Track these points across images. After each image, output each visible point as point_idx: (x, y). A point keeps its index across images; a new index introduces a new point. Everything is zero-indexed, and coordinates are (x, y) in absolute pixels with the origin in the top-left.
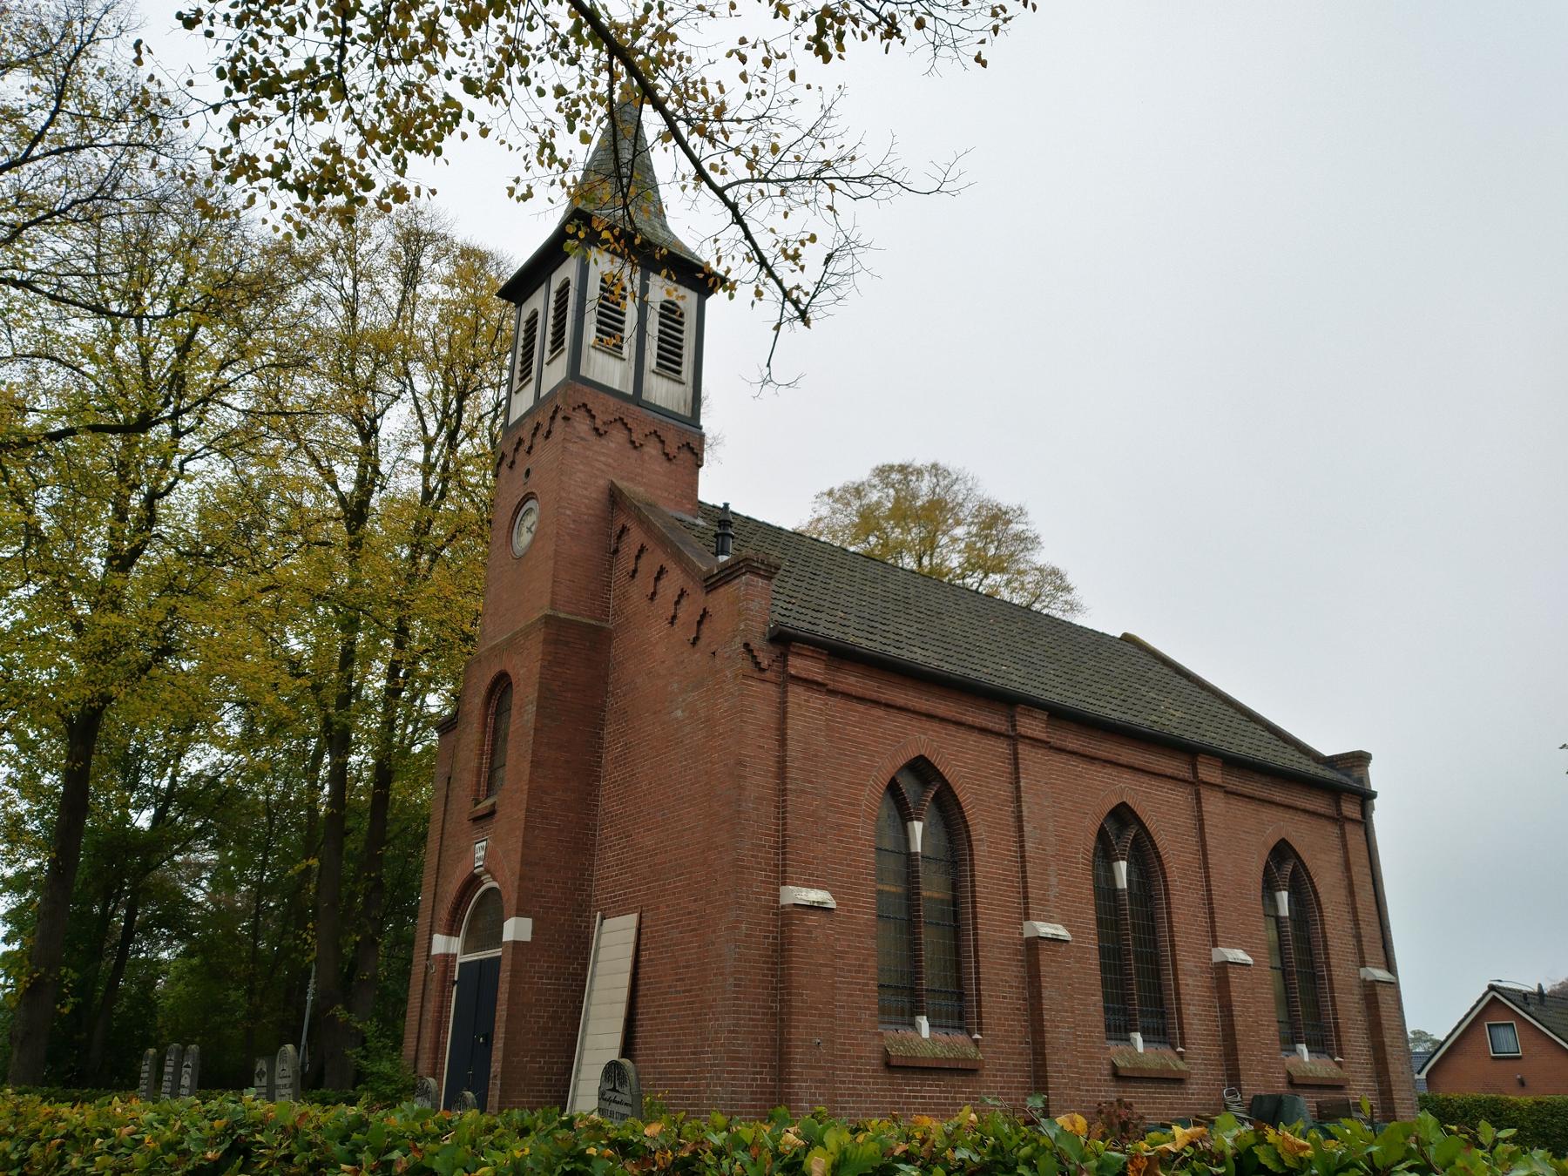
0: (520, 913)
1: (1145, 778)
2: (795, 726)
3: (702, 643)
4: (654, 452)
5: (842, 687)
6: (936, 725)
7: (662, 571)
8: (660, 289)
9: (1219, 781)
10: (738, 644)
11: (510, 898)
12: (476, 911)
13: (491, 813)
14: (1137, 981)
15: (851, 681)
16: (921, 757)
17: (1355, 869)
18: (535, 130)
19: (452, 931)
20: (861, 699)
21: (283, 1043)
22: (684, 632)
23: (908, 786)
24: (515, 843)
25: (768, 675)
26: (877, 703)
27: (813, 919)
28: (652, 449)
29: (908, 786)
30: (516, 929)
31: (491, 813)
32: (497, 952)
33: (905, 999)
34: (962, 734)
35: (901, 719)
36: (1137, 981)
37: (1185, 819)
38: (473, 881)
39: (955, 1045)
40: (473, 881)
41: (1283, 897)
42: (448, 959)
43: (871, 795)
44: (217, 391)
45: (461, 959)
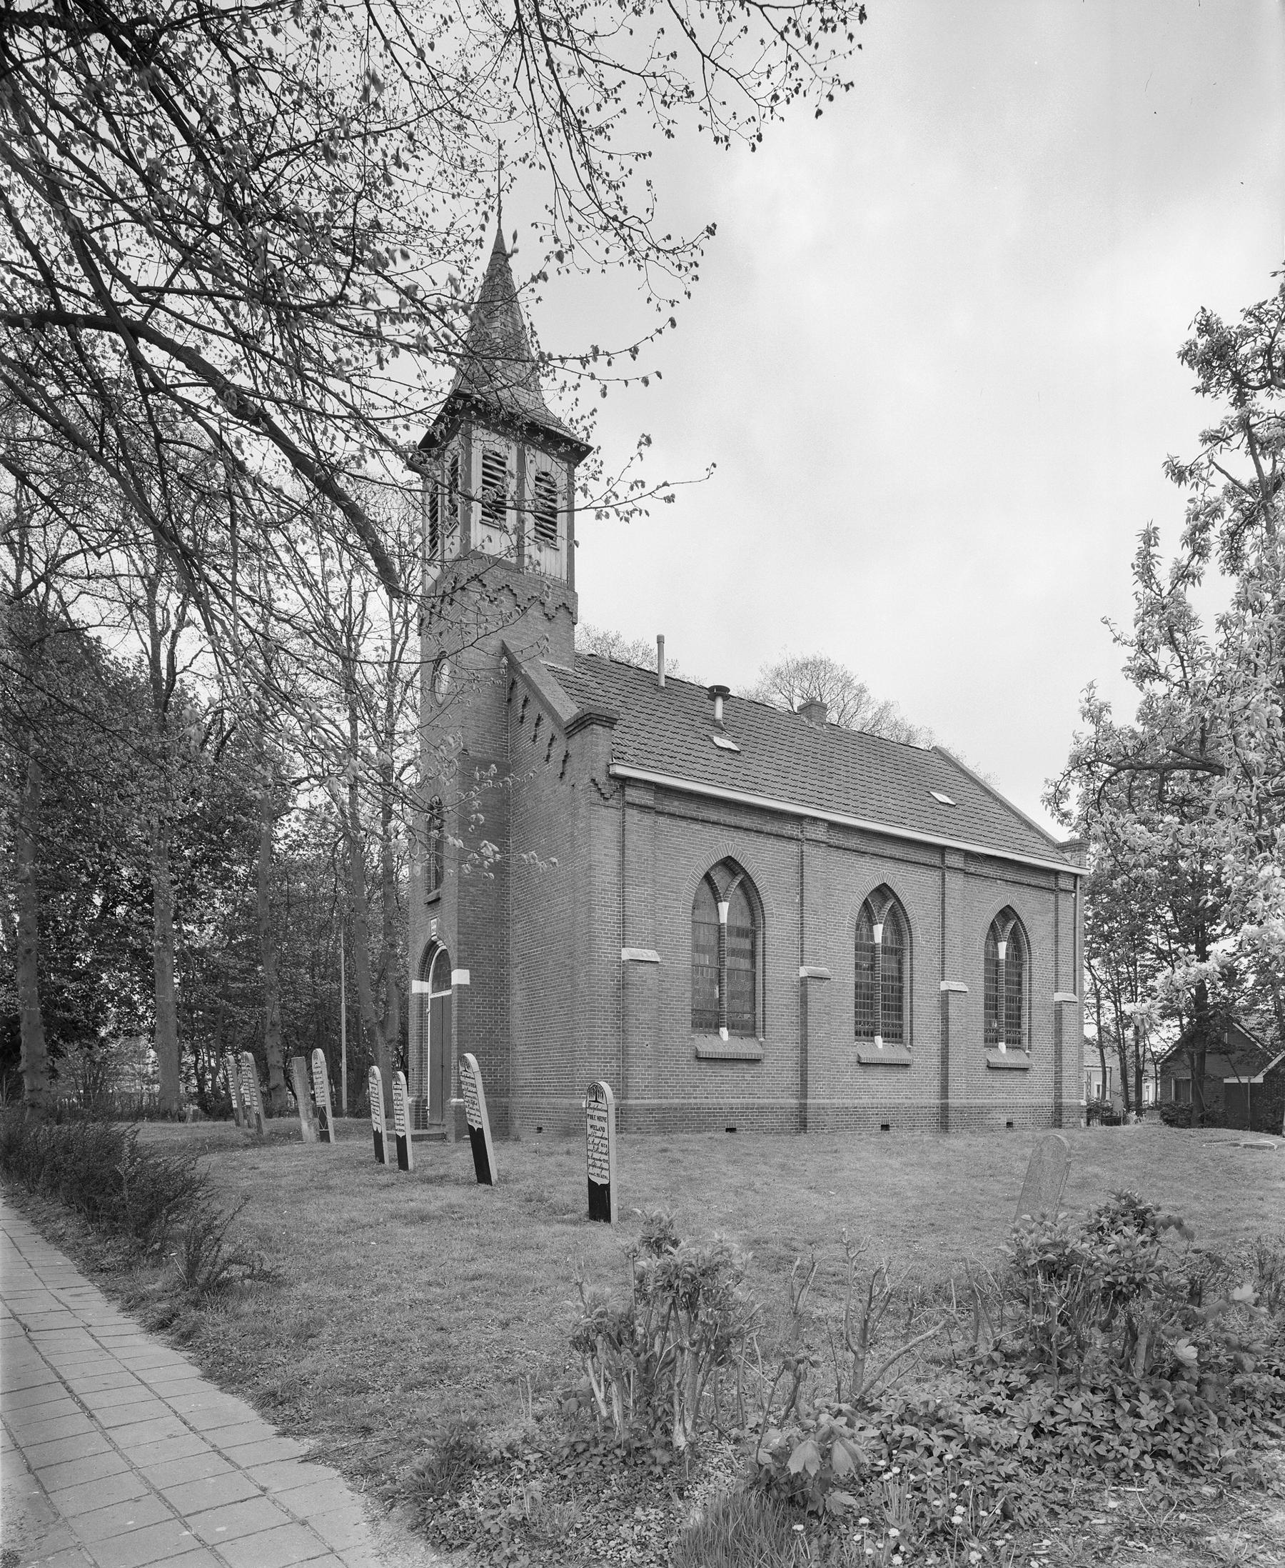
0: (460, 966)
1: (903, 866)
2: (632, 838)
3: (567, 777)
4: (536, 614)
5: (667, 809)
6: (741, 834)
7: (539, 719)
8: (540, 461)
9: (961, 866)
10: (587, 780)
11: (453, 955)
12: (436, 963)
13: (438, 900)
14: (882, 1006)
15: (675, 806)
16: (729, 857)
17: (1061, 925)
18: (600, 131)
19: (423, 977)
20: (683, 818)
21: (313, 1048)
22: (554, 767)
23: (720, 878)
24: (453, 919)
25: (611, 802)
26: (695, 820)
27: (642, 969)
28: (535, 612)
29: (720, 878)
30: (460, 977)
31: (438, 900)
32: (448, 992)
33: (707, 1020)
34: (761, 839)
35: (716, 831)
36: (882, 1006)
37: (933, 895)
38: (432, 946)
39: (746, 1047)
40: (432, 946)
41: (1003, 946)
42: (422, 997)
43: (690, 883)
44: (367, 424)
45: (431, 996)
